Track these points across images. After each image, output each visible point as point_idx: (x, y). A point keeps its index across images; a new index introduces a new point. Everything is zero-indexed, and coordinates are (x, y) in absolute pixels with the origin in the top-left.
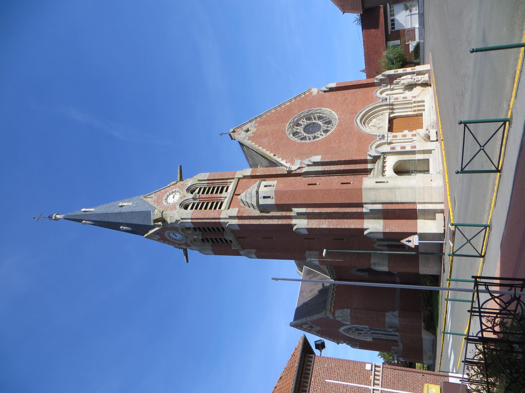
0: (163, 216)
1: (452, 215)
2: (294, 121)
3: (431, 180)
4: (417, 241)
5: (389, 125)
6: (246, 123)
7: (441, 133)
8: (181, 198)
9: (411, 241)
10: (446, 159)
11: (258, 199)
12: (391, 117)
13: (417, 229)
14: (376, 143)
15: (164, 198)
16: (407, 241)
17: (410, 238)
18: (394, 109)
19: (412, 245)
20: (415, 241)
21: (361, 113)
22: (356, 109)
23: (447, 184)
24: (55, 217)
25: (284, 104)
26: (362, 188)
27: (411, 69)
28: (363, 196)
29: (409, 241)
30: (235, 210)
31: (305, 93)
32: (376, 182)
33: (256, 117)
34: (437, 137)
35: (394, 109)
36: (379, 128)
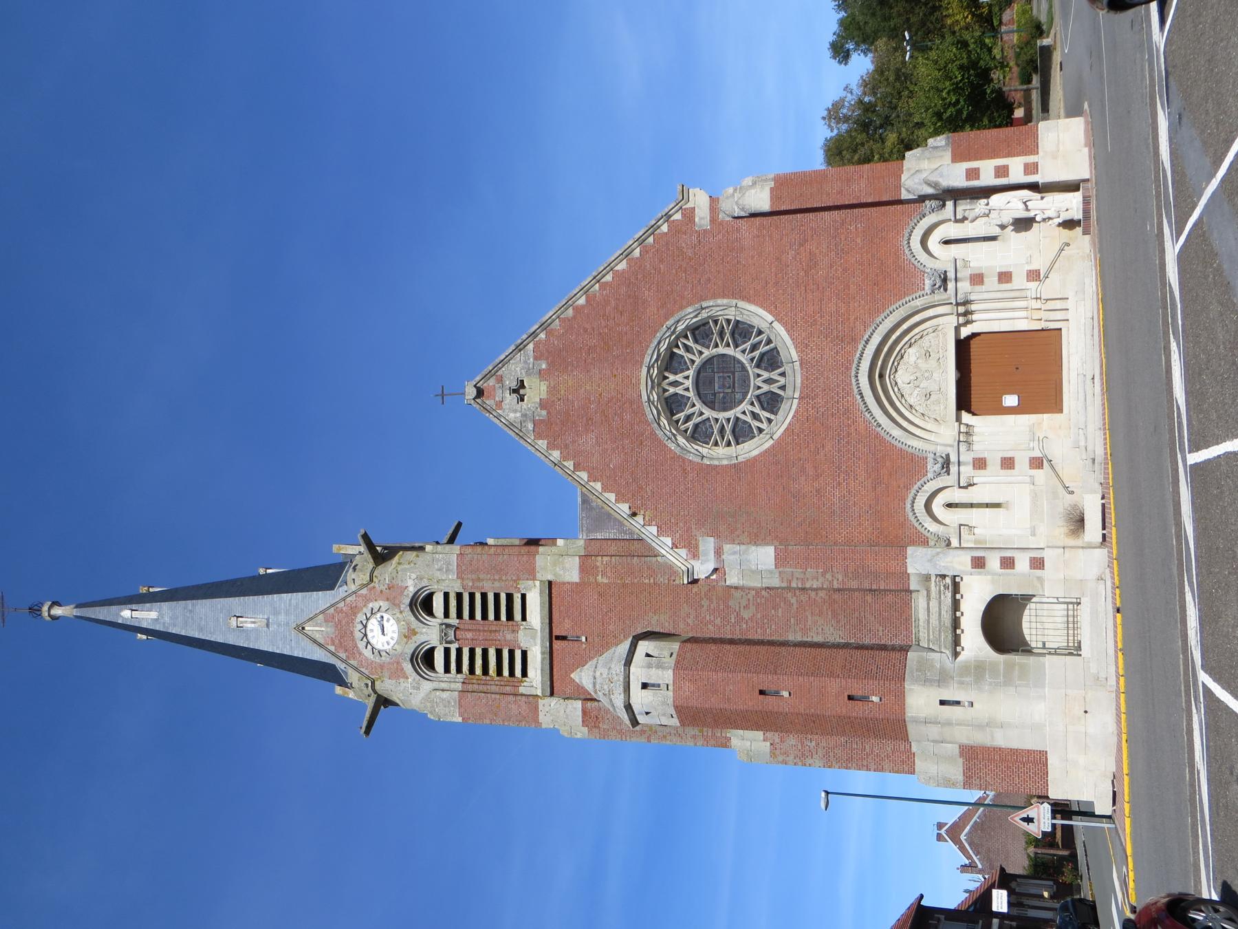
0: (379, 693)
1: (1133, 878)
2: (659, 355)
3: (1086, 712)
4: (1047, 822)
5: (959, 375)
6: (507, 356)
7: (1127, 798)
8: (405, 637)
9: (1033, 818)
10: (1134, 868)
11: (633, 717)
12: (962, 338)
13: (1047, 786)
14: (925, 487)
15: (358, 635)
16: (1024, 819)
17: (1031, 812)
18: (972, 313)
19: (1036, 831)
20: (1042, 821)
21: (867, 342)
22: (852, 318)
23: (1123, 716)
24: (49, 615)
25: (610, 268)
26: (905, 720)
27: (1022, 168)
28: (909, 732)
29: (1029, 820)
30: (575, 708)
31: (671, 216)
32: (942, 703)
33: (534, 332)
34: (1104, 528)
35: (972, 313)
36: (928, 396)
